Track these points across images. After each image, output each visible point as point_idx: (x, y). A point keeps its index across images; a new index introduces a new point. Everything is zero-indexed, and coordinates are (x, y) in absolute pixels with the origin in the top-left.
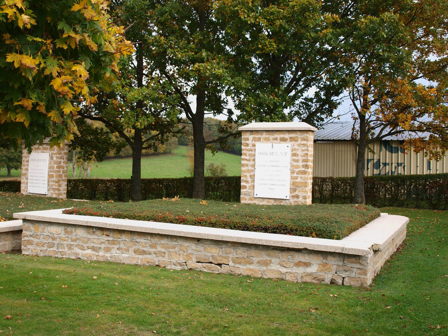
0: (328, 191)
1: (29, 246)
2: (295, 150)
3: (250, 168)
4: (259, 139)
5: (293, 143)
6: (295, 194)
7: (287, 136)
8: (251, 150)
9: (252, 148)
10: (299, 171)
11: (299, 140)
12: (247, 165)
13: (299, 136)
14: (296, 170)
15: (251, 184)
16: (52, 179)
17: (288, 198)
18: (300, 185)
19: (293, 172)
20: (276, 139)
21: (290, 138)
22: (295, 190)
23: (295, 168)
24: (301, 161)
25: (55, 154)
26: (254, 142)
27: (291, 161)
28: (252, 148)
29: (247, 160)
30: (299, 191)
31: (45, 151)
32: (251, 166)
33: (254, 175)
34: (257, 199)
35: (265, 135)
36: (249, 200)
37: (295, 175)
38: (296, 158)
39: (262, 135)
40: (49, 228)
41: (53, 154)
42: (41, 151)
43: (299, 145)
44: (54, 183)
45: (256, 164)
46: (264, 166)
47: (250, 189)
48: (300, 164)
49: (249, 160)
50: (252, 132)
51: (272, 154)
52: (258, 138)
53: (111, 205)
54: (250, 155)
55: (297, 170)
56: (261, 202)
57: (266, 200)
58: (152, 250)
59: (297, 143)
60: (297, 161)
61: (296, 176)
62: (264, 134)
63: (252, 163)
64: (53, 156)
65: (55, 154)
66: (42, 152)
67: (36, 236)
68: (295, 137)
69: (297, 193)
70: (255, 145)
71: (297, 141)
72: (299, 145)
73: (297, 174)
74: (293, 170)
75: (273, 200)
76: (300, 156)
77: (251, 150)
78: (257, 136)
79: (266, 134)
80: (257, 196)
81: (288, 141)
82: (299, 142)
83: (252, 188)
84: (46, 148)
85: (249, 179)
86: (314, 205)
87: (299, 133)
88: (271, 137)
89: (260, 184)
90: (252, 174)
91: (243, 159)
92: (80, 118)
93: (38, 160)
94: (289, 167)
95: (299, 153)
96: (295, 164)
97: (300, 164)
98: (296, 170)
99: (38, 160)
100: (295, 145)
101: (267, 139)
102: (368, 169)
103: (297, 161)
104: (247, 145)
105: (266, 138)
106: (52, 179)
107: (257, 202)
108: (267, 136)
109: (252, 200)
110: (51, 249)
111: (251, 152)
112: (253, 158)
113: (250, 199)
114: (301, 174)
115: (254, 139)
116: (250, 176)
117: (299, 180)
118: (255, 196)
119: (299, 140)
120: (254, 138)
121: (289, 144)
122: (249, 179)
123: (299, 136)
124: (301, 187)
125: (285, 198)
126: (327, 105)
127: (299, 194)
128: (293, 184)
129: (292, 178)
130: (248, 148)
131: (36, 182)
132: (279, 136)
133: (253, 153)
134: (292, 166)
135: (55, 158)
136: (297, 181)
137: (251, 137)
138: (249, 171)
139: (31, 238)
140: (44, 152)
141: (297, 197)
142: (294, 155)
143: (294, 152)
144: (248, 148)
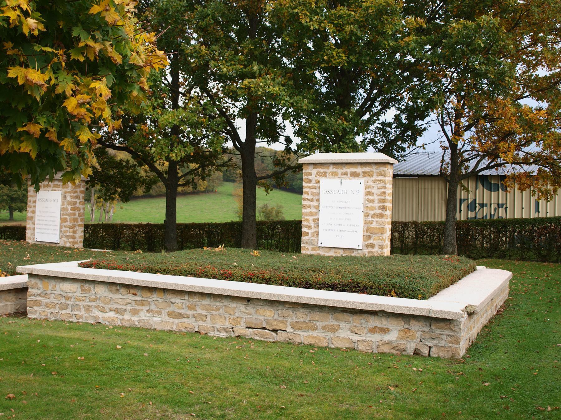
0: (410, 239)
1: (36, 308)
2: (369, 187)
3: (313, 210)
4: (325, 174)
5: (367, 178)
6: (369, 242)
7: (359, 170)
8: (314, 188)
9: (316, 185)
10: (374, 214)
11: (375, 174)
12: (309, 207)
13: (374, 170)
14: (370, 212)
15: (314, 230)
16: (65, 224)
17: (360, 248)
18: (375, 231)
19: (366, 215)
20: (346, 174)
21: (364, 172)
22: (369, 238)
23: (370, 210)
24: (376, 201)
25: (69, 192)
26: (318, 178)
27: (365, 201)
28: (316, 185)
29: (309, 200)
30: (374, 239)
31: (56, 189)
32: (315, 207)
33: (318, 219)
34: (322, 249)
35: (331, 169)
36: (312, 250)
37: (370, 218)
38: (370, 197)
39: (328, 169)
40: (61, 285)
41: (66, 192)
42: (51, 188)
43: (374, 182)
44: (68, 229)
45: (320, 206)
46: (331, 207)
47: (313, 236)
48: (376, 205)
49: (312, 200)
50: (315, 164)
51: (340, 192)
52: (323, 172)
53: (140, 256)
54: (313, 194)
55: (372, 212)
56: (326, 252)
57: (334, 250)
58: (191, 313)
59: (371, 179)
60: (372, 201)
61: (370, 220)
62: (331, 167)
63: (315, 203)
64: (67, 195)
65: (69, 192)
66: (52, 190)
67: (45, 295)
68: (369, 172)
69: (372, 241)
70: (319, 182)
71: (372, 176)
72: (374, 182)
73: (372, 217)
74: (367, 213)
75: (342, 250)
76: (375, 196)
77: (314, 188)
78: (322, 170)
79: (333, 168)
80: (322, 245)
81: (361, 176)
82: (375, 177)
83: (315, 235)
84: (57, 185)
85: (312, 224)
86: (393, 256)
87: (374, 167)
88: (340, 171)
89: (326, 230)
90: (316, 217)
91: (305, 199)
92: (100, 147)
93: (47, 200)
94: (362, 209)
95: (375, 191)
96: (369, 205)
97: (376, 205)
98: (370, 212)
99: (47, 200)
100: (369, 181)
101: (334, 174)
102: (461, 211)
103: (372, 201)
104: (310, 181)
105: (333, 172)
106: (65, 224)
107: (322, 253)
108: (335, 170)
109: (315, 250)
110: (64, 311)
111: (314, 190)
112: (317, 197)
113: (313, 249)
114: (377, 218)
115: (318, 174)
116: (314, 220)
117: (374, 225)
118: (320, 245)
119: (375, 174)
120: (318, 172)
121: (362, 180)
122: (312, 224)
123: (374, 170)
124: (377, 234)
125: (357, 248)
126: (410, 131)
127: (375, 242)
128: (367, 230)
129: (366, 223)
130: (310, 185)
131: (45, 227)
132: (349, 170)
133: (317, 191)
134: (366, 207)
135: (68, 198)
136: (371, 226)
137: (314, 171)
138: (311, 214)
139: (39, 298)
140: (55, 190)
141: (372, 246)
142: (368, 193)
143: (368, 190)
144: (310, 185)
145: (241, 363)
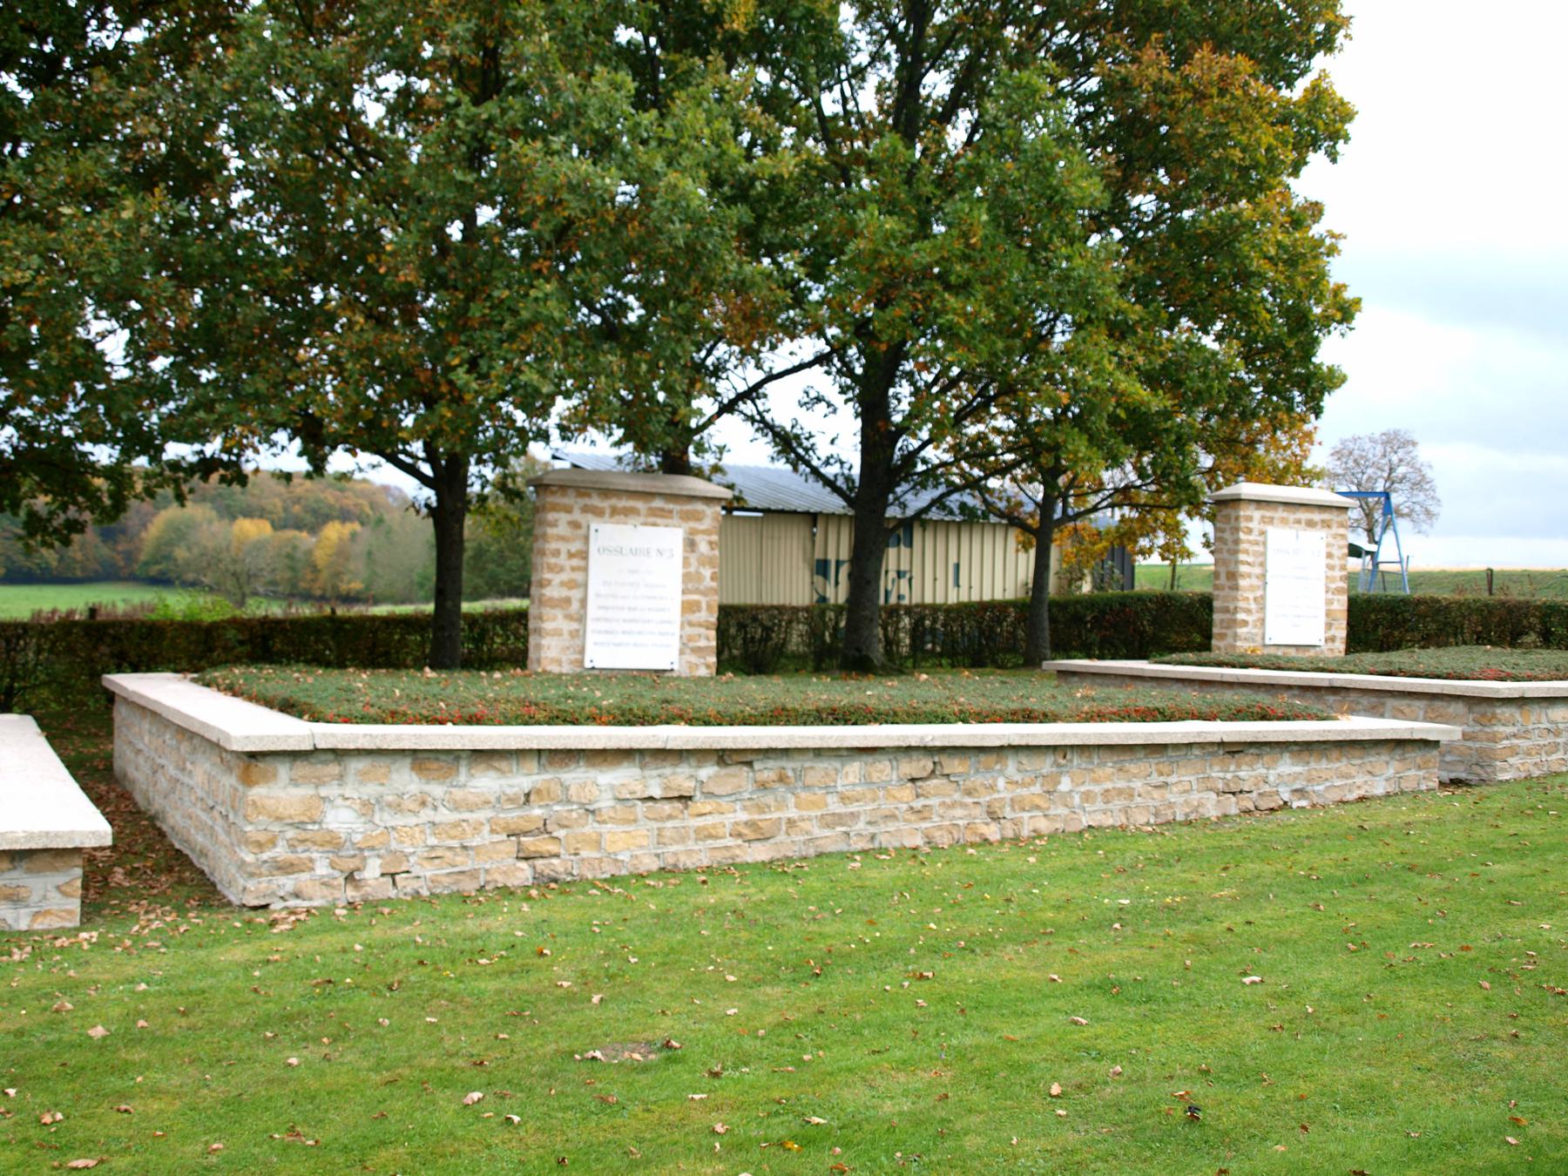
0: (748, 642)
1: (1511, 760)
3: (1255, 582)
7: (1317, 516)
9: (1261, 539)
12: (1249, 576)
16: (695, 617)
20: (1298, 522)
21: (1323, 521)
25: (704, 532)
26: (1262, 527)
28: (1261, 539)
31: (659, 521)
33: (1263, 597)
40: (1550, 712)
41: (693, 532)
42: (642, 519)
44: (702, 631)
50: (1259, 503)
53: (969, 686)
54: (1256, 554)
58: (969, 800)
62: (1281, 508)
64: (698, 538)
65: (704, 532)
66: (645, 524)
67: (1525, 735)
78: (1268, 514)
84: (662, 510)
85: (1253, 606)
86: (1351, 657)
87: (1335, 513)
91: (1243, 563)
93: (634, 552)
96: (1330, 573)
99: (634, 552)
101: (1284, 521)
102: (837, 583)
104: (1250, 531)
106: (695, 617)
107: (1272, 651)
108: (1285, 514)
110: (1554, 757)
111: (1256, 548)
112: (1260, 559)
115: (1263, 520)
122: (1253, 606)
130: (1251, 538)
131: (627, 627)
132: (1304, 515)
133: (1261, 549)
135: (703, 547)
137: (1257, 514)
138: (1252, 588)
139: (1515, 741)
140: (655, 525)
144: (1251, 538)
145: (420, 969)
